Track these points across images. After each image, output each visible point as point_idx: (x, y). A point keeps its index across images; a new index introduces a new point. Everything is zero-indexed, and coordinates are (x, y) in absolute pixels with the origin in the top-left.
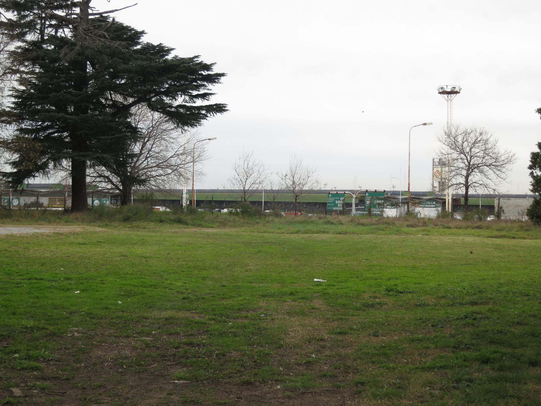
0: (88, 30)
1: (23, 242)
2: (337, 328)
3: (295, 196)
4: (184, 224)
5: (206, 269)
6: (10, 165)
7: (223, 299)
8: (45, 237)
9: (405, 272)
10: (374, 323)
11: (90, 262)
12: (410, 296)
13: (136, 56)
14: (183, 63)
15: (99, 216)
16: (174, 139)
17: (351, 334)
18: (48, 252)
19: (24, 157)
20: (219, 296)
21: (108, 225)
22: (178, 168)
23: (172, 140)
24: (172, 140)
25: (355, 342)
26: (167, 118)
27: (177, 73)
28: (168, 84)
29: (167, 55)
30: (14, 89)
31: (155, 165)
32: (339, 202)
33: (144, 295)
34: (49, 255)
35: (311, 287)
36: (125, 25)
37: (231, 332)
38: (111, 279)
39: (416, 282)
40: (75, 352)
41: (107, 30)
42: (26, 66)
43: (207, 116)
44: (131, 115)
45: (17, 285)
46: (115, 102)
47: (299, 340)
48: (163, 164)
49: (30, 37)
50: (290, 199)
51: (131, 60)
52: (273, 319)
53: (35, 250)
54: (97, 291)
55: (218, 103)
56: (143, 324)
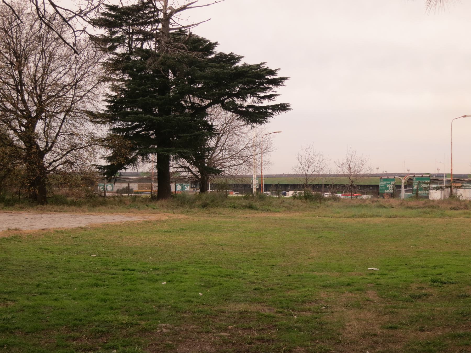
0: (169, 43)
1: (117, 231)
2: (389, 322)
3: (351, 182)
4: (254, 210)
5: (274, 257)
6: (105, 159)
7: (289, 289)
8: (135, 225)
9: (448, 259)
10: (420, 317)
11: (174, 251)
12: (452, 286)
13: (211, 64)
14: (252, 69)
15: (182, 203)
16: (245, 133)
17: (400, 329)
18: (139, 241)
19: (116, 153)
20: (286, 287)
21: (189, 212)
22: (249, 159)
23: (243, 135)
24: (243, 135)
25: (404, 338)
26: (239, 117)
27: (247, 78)
28: (238, 87)
29: (237, 62)
30: (107, 95)
31: (228, 156)
32: (390, 186)
33: (221, 286)
34: (139, 244)
35: (365, 277)
36: (200, 37)
37: (296, 327)
38: (193, 269)
39: (458, 270)
40: (164, 348)
41: (186, 43)
42: (117, 75)
43: (272, 114)
44: (207, 115)
45: (113, 276)
46: (193, 104)
47: (355, 335)
48: (236, 156)
49: (120, 50)
50: (346, 182)
51: (206, 68)
52: (332, 312)
53: (128, 239)
54: (181, 282)
55: (282, 103)
56: (221, 319)
